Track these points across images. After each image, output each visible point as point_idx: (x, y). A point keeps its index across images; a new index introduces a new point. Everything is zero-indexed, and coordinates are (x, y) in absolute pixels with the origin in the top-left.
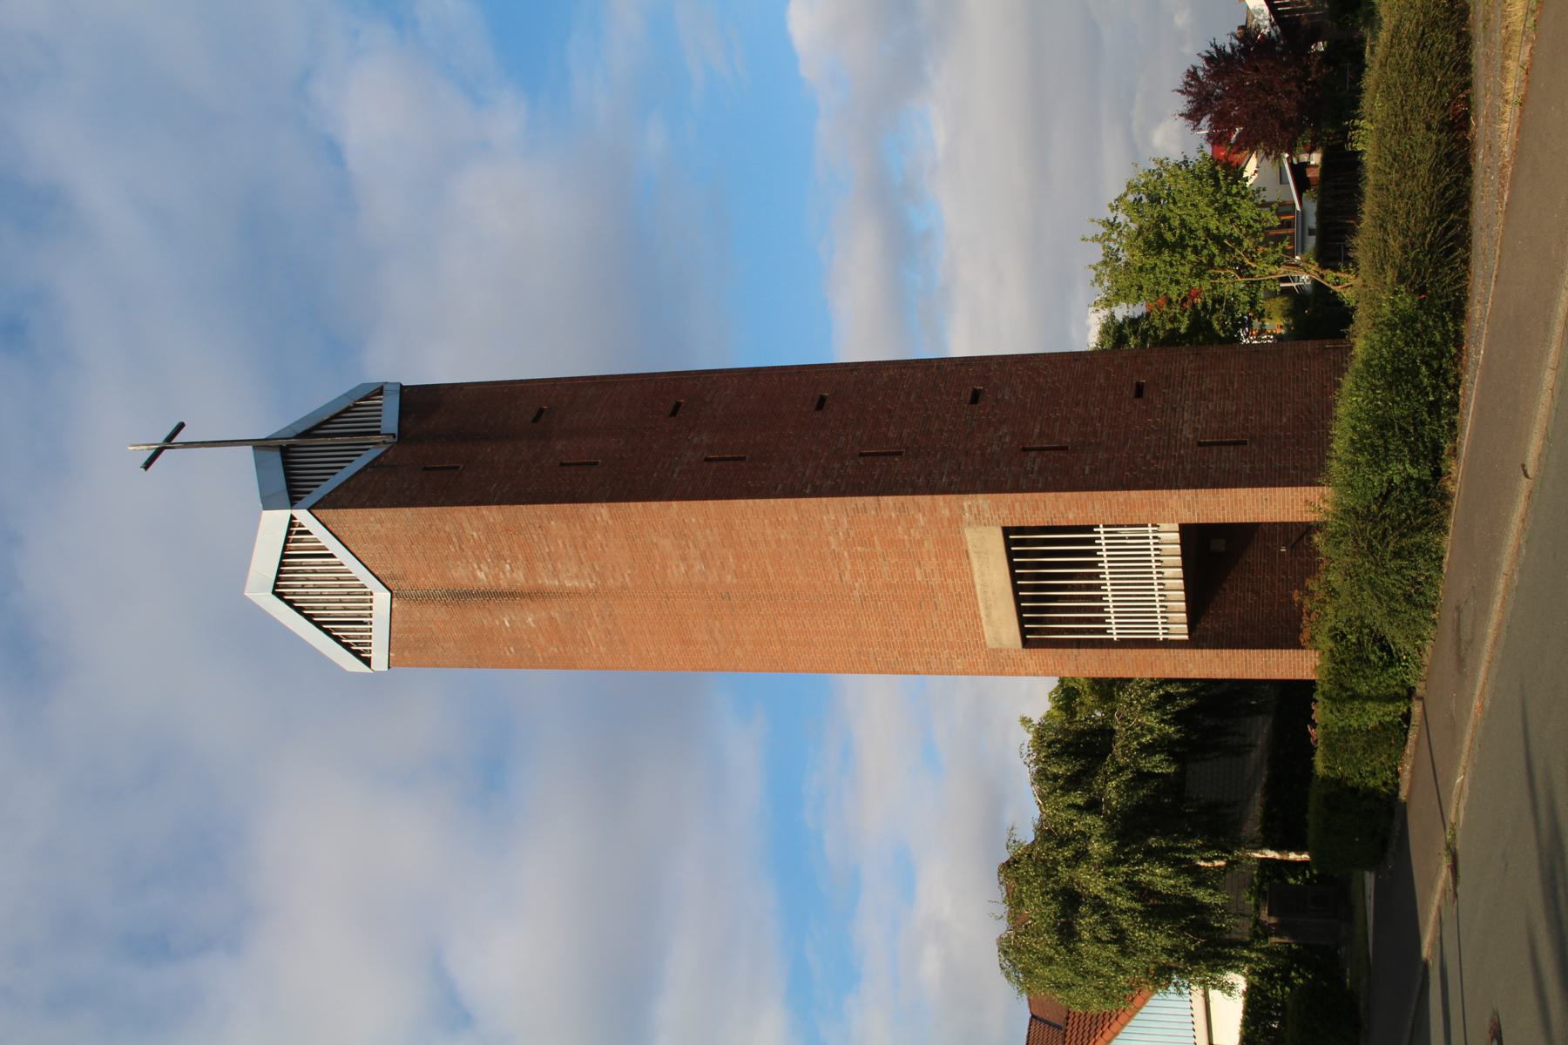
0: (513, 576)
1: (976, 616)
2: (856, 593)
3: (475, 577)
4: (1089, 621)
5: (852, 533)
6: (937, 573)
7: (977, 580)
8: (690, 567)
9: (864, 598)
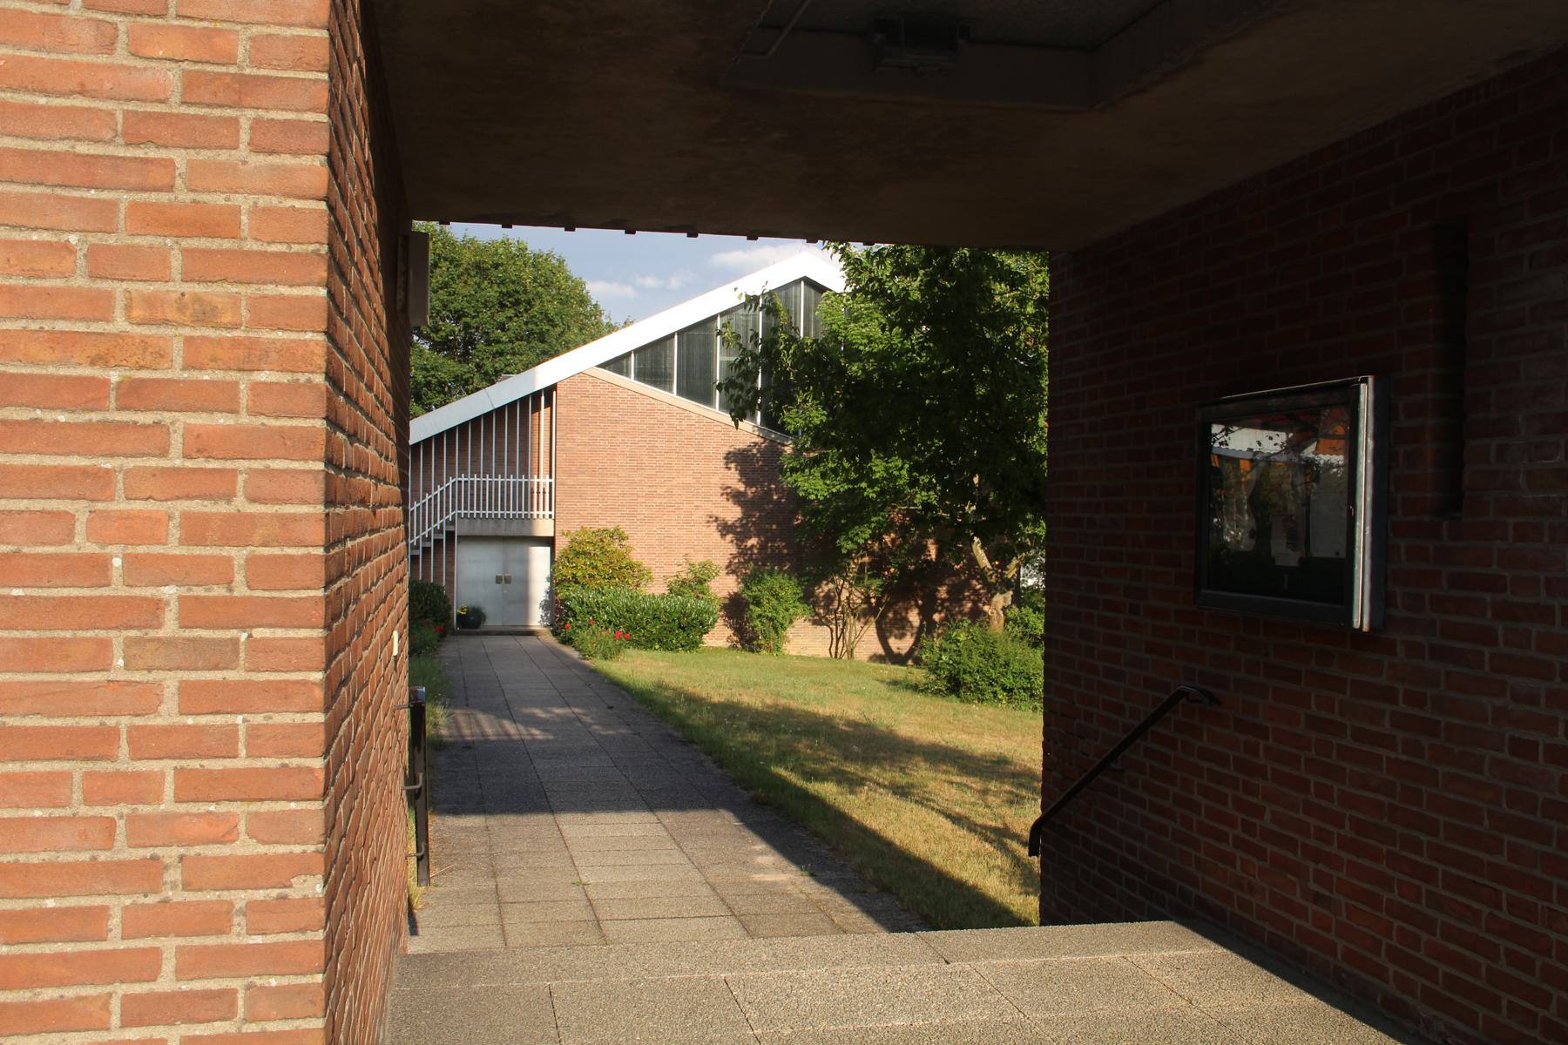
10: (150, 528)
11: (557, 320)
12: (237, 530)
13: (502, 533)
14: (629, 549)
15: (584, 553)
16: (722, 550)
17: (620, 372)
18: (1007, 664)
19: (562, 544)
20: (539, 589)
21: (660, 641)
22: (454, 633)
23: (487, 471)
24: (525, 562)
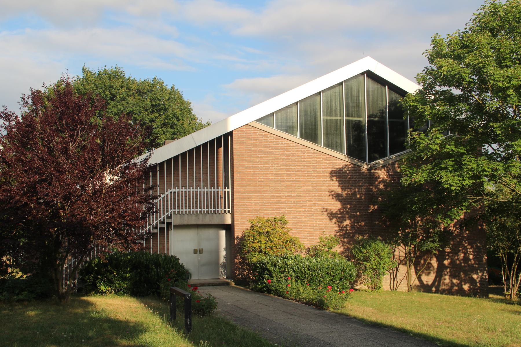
11: (180, 118)
16: (331, 228)
17: (268, 124)
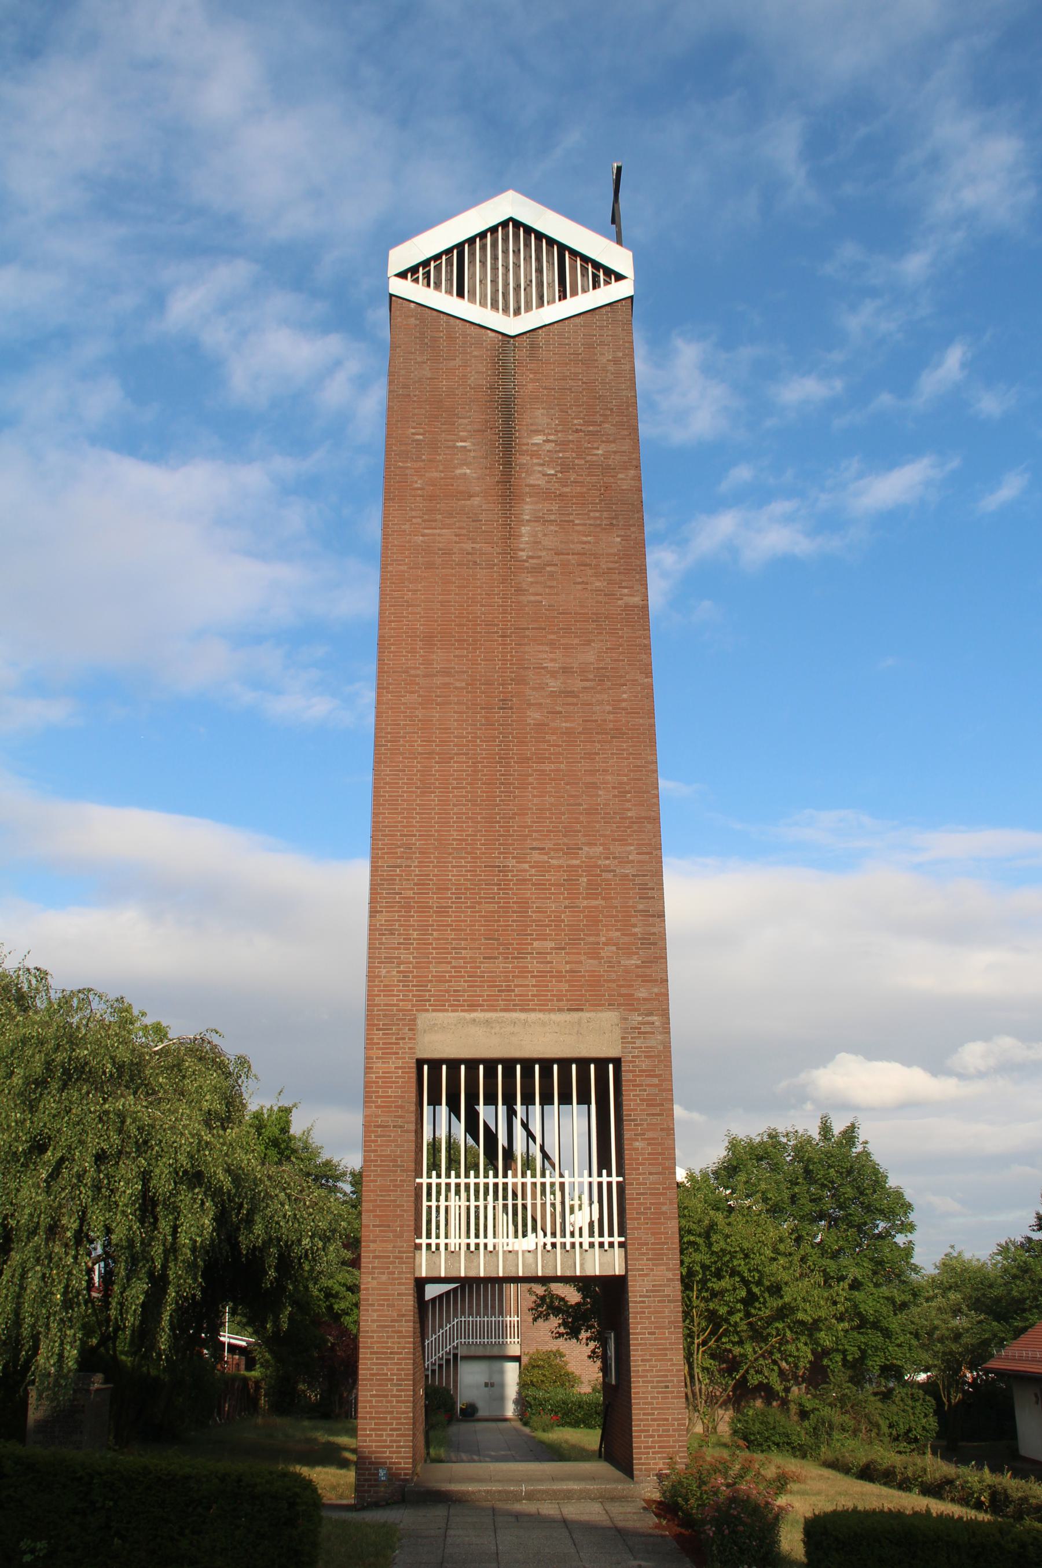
0: (536, 474)
1: (473, 1007)
2: (511, 863)
3: (537, 432)
4: (477, 1218)
5: (610, 876)
6: (542, 967)
7: (533, 1016)
8: (553, 674)
9: (504, 870)
10: (392, 1370)
12: (403, 1369)
13: (488, 1354)
14: (566, 1363)
15: (538, 1366)
18: (774, 1428)
19: (525, 1360)
20: (512, 1390)
21: (584, 1422)
22: (459, 1420)
23: (478, 1314)
24: (502, 1372)
